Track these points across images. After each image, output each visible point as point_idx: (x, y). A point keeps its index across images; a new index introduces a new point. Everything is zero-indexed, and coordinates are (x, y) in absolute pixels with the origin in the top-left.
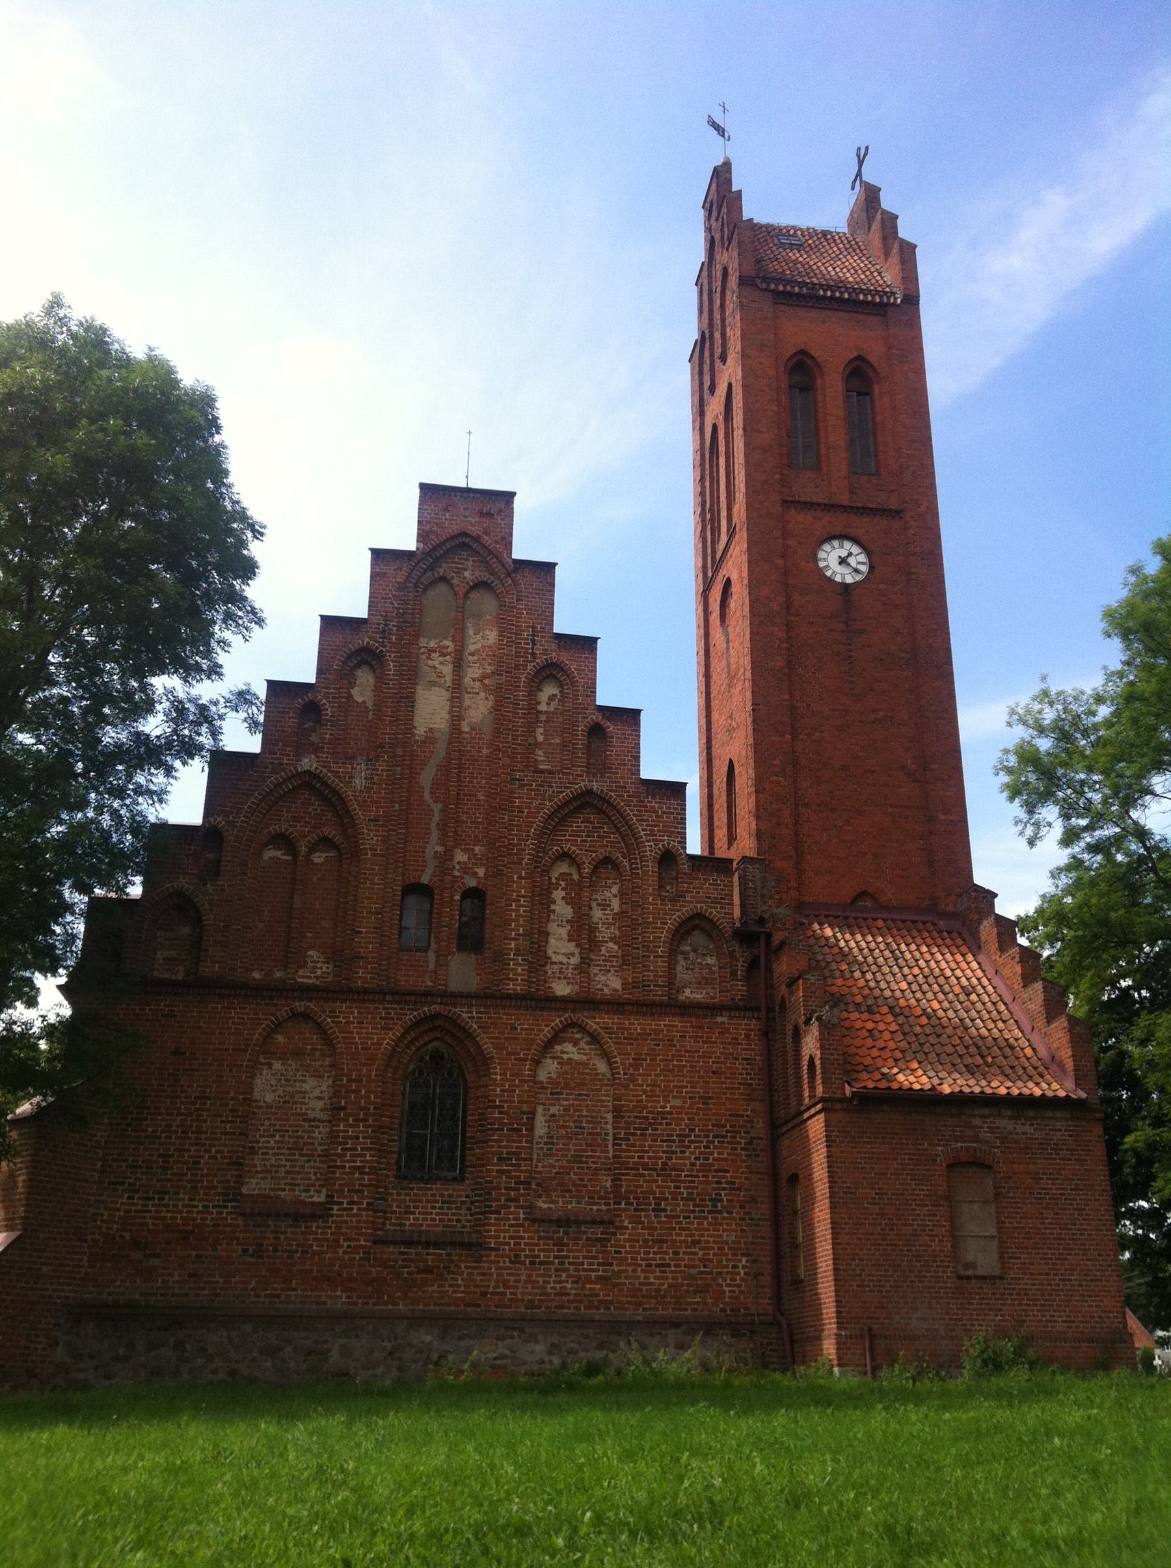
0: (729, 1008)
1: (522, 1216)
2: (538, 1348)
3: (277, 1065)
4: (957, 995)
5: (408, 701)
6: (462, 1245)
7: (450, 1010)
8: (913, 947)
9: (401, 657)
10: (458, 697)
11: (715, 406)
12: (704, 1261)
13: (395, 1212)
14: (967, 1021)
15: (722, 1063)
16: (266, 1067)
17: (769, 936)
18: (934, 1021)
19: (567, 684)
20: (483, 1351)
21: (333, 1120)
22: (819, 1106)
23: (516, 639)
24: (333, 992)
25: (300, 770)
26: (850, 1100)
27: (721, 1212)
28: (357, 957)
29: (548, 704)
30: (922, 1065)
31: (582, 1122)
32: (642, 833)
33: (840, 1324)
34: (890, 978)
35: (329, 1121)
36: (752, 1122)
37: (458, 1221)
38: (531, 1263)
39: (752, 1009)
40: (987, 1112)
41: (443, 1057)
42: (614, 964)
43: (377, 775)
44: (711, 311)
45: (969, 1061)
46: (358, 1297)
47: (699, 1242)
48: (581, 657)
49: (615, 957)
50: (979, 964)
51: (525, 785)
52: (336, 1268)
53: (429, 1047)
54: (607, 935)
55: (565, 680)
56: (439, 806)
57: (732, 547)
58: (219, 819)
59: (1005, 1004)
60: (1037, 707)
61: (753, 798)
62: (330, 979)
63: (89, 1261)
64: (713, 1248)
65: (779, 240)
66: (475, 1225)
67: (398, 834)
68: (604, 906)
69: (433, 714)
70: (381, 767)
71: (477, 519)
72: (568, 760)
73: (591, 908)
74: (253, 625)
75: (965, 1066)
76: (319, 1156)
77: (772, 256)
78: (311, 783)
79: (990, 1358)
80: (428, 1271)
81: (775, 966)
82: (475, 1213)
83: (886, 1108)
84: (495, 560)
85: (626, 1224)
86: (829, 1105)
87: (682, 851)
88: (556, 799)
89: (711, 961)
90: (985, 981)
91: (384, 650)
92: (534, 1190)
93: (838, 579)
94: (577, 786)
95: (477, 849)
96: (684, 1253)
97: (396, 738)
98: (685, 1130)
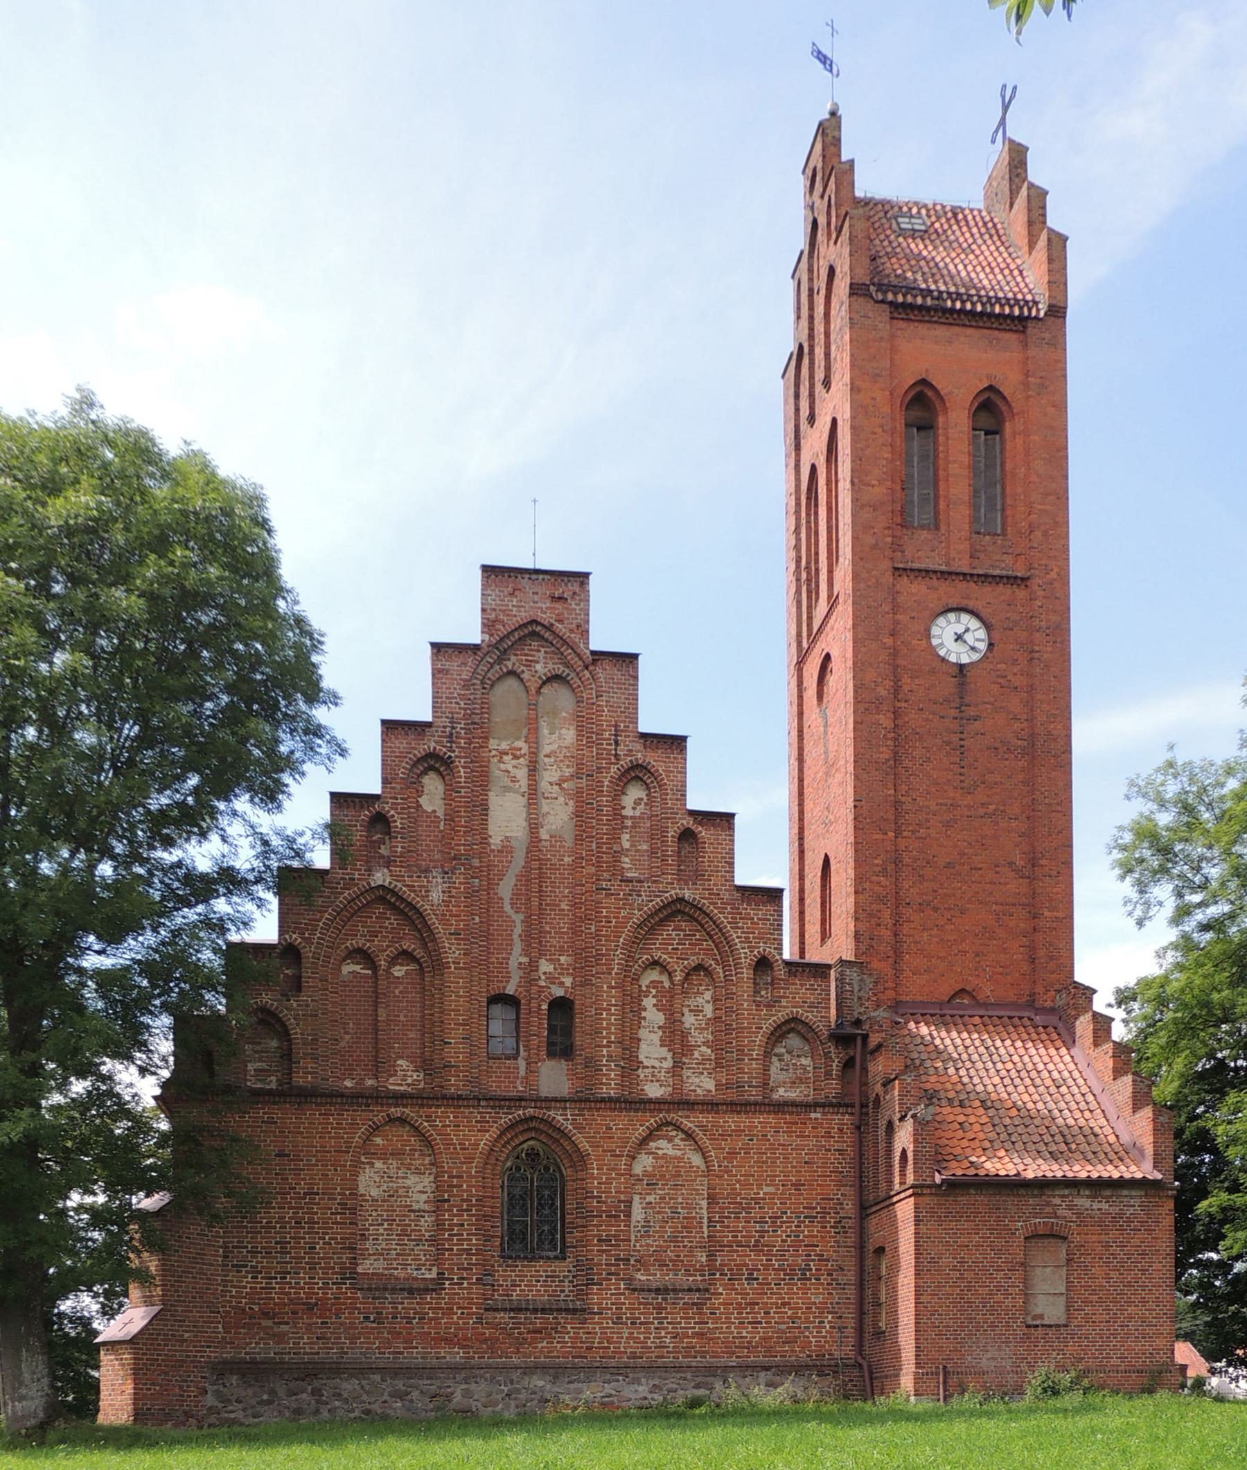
0: (823, 1105)
1: (622, 1286)
2: (641, 1388)
3: (379, 1164)
4: (1047, 1088)
5: (482, 809)
6: (567, 1310)
7: (545, 1114)
8: (1008, 1042)
9: (472, 762)
10: (535, 804)
11: (815, 442)
12: (793, 1319)
13: (502, 1285)
14: (1056, 1112)
15: (815, 1154)
16: (367, 1166)
17: (865, 1038)
18: (1024, 1113)
19: (655, 787)
20: (591, 1392)
21: (437, 1211)
22: (910, 1191)
23: (597, 739)
24: (428, 1098)
25: (373, 885)
26: (940, 1186)
27: (810, 1279)
28: (447, 1066)
29: (634, 809)
30: (1009, 1153)
31: (677, 1208)
32: (737, 941)
33: (918, 1365)
34: (983, 1073)
35: (434, 1212)
36: (842, 1204)
37: (563, 1291)
38: (632, 1323)
39: (847, 1106)
40: (1066, 1192)
41: (538, 1154)
42: (708, 1066)
43: (454, 888)
44: (811, 318)
45: (1053, 1148)
46: (474, 1353)
47: (789, 1303)
48: (669, 758)
49: (707, 1060)
50: (1072, 1057)
51: (612, 894)
52: (452, 1330)
53: (525, 1146)
54: (700, 1040)
55: (652, 782)
56: (521, 917)
57: (833, 617)
58: (294, 936)
59: (1094, 1095)
60: (1160, 778)
61: (852, 899)
62: (422, 1086)
63: (223, 1328)
64: (802, 1308)
65: (898, 224)
66: (578, 1295)
67: (480, 946)
68: (697, 1011)
69: (508, 821)
70: (458, 879)
71: (548, 605)
72: (658, 867)
73: (683, 1015)
74: (337, 757)
75: (1050, 1153)
76: (426, 1240)
77: (889, 249)
78: (385, 897)
79: (1049, 1386)
80: (535, 1332)
81: (871, 1067)
82: (577, 1285)
83: (973, 1191)
84: (570, 651)
85: (720, 1290)
86: (918, 1190)
87: (778, 957)
88: (645, 908)
89: (804, 1061)
90: (1076, 1074)
91: (453, 755)
92: (633, 1266)
93: (953, 659)
94: (667, 895)
95: (563, 959)
96: (775, 1313)
97: (472, 849)
98: (777, 1213)
